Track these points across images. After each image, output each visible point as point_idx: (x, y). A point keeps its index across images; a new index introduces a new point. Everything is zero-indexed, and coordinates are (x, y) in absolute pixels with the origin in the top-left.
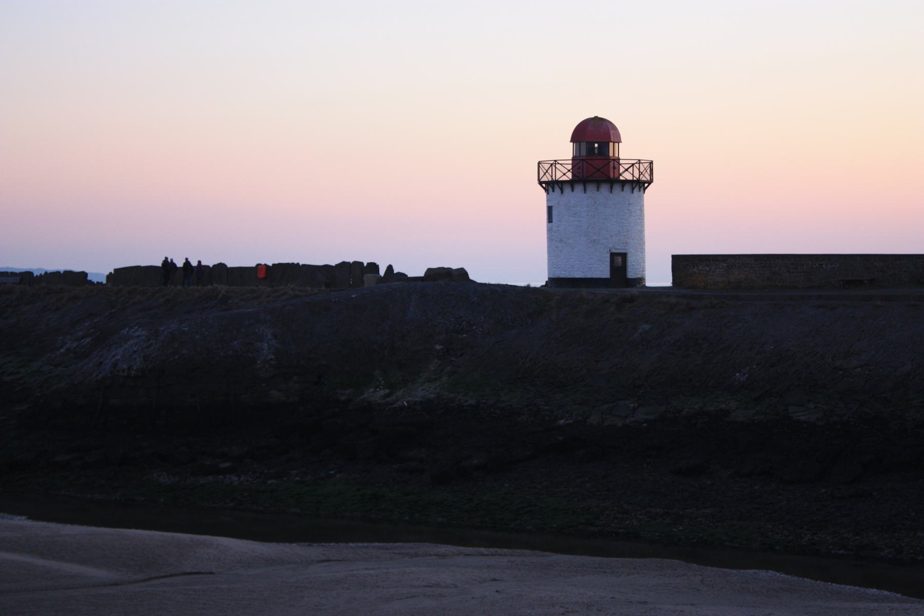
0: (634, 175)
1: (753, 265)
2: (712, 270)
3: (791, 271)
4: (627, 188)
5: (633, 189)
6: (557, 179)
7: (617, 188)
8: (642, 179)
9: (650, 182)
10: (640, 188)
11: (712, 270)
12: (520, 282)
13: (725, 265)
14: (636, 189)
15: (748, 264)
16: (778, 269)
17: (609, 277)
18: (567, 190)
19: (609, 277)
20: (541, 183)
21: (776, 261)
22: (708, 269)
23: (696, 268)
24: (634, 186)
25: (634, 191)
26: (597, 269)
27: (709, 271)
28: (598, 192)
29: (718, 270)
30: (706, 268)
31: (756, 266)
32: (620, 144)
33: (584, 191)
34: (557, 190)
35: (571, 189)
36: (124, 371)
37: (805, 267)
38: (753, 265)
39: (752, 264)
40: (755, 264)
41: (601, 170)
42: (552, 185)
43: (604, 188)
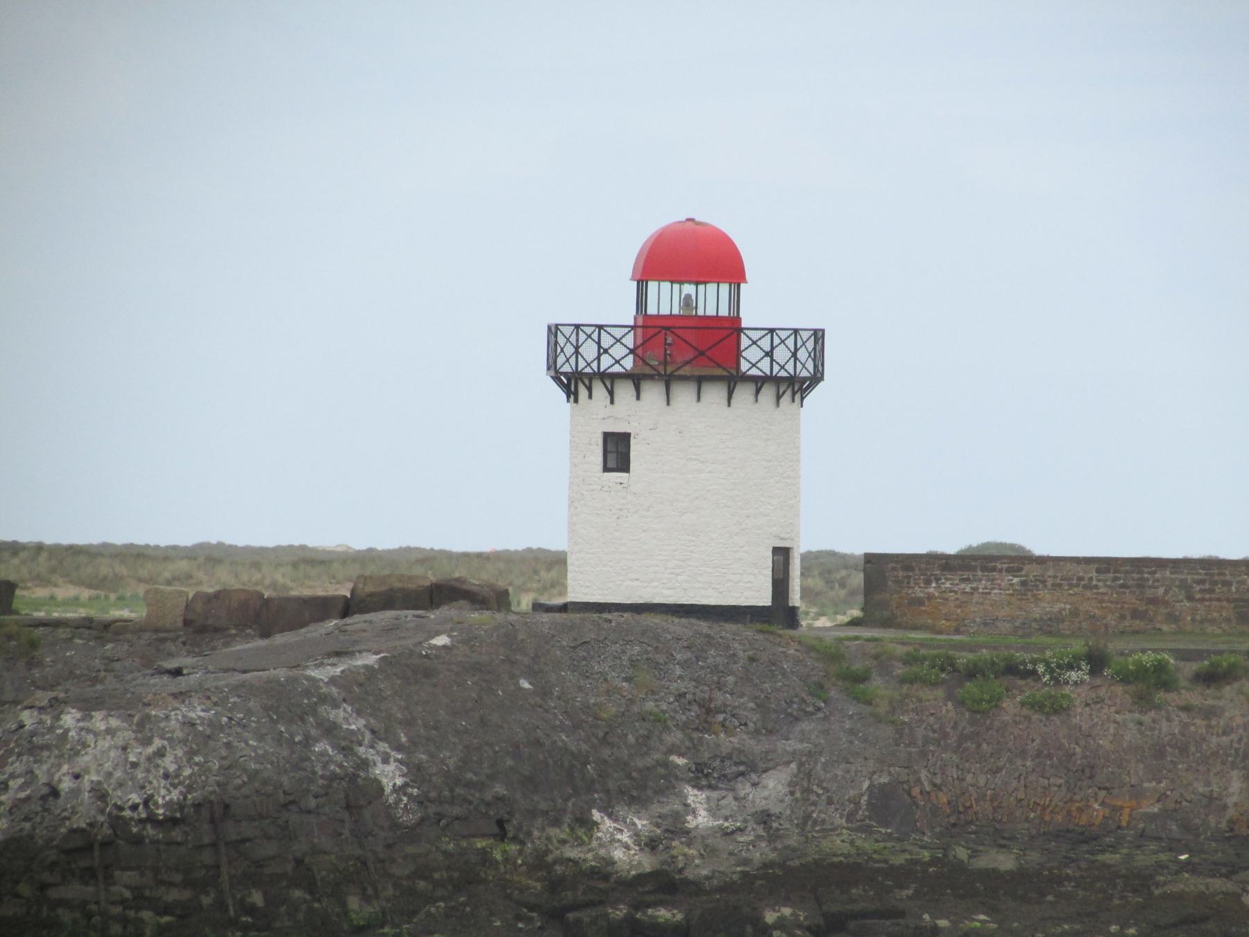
0: (596, 346)
1: (1094, 583)
2: (980, 590)
3: (1198, 596)
4: (768, 393)
5: (779, 397)
6: (602, 370)
7: (744, 394)
8: (802, 375)
9: (817, 378)
10: (794, 394)
11: (980, 590)
12: (761, 604)
13: (1016, 580)
14: (787, 398)
15: (1080, 579)
16: (1161, 591)
17: (770, 604)
18: (625, 391)
19: (770, 604)
20: (556, 379)
21: (1158, 575)
22: (968, 590)
23: (934, 585)
24: (781, 392)
25: (782, 400)
26: (750, 585)
27: (972, 594)
28: (757, 405)
29: (995, 591)
30: (963, 586)
31: (1100, 584)
32: (742, 285)
33: (727, 403)
34: (599, 390)
35: (634, 393)
36: (134, 807)
37: (1233, 589)
38: (1094, 583)
39: (1091, 579)
40: (1099, 580)
41: (708, 353)
42: (587, 382)
43: (714, 394)
